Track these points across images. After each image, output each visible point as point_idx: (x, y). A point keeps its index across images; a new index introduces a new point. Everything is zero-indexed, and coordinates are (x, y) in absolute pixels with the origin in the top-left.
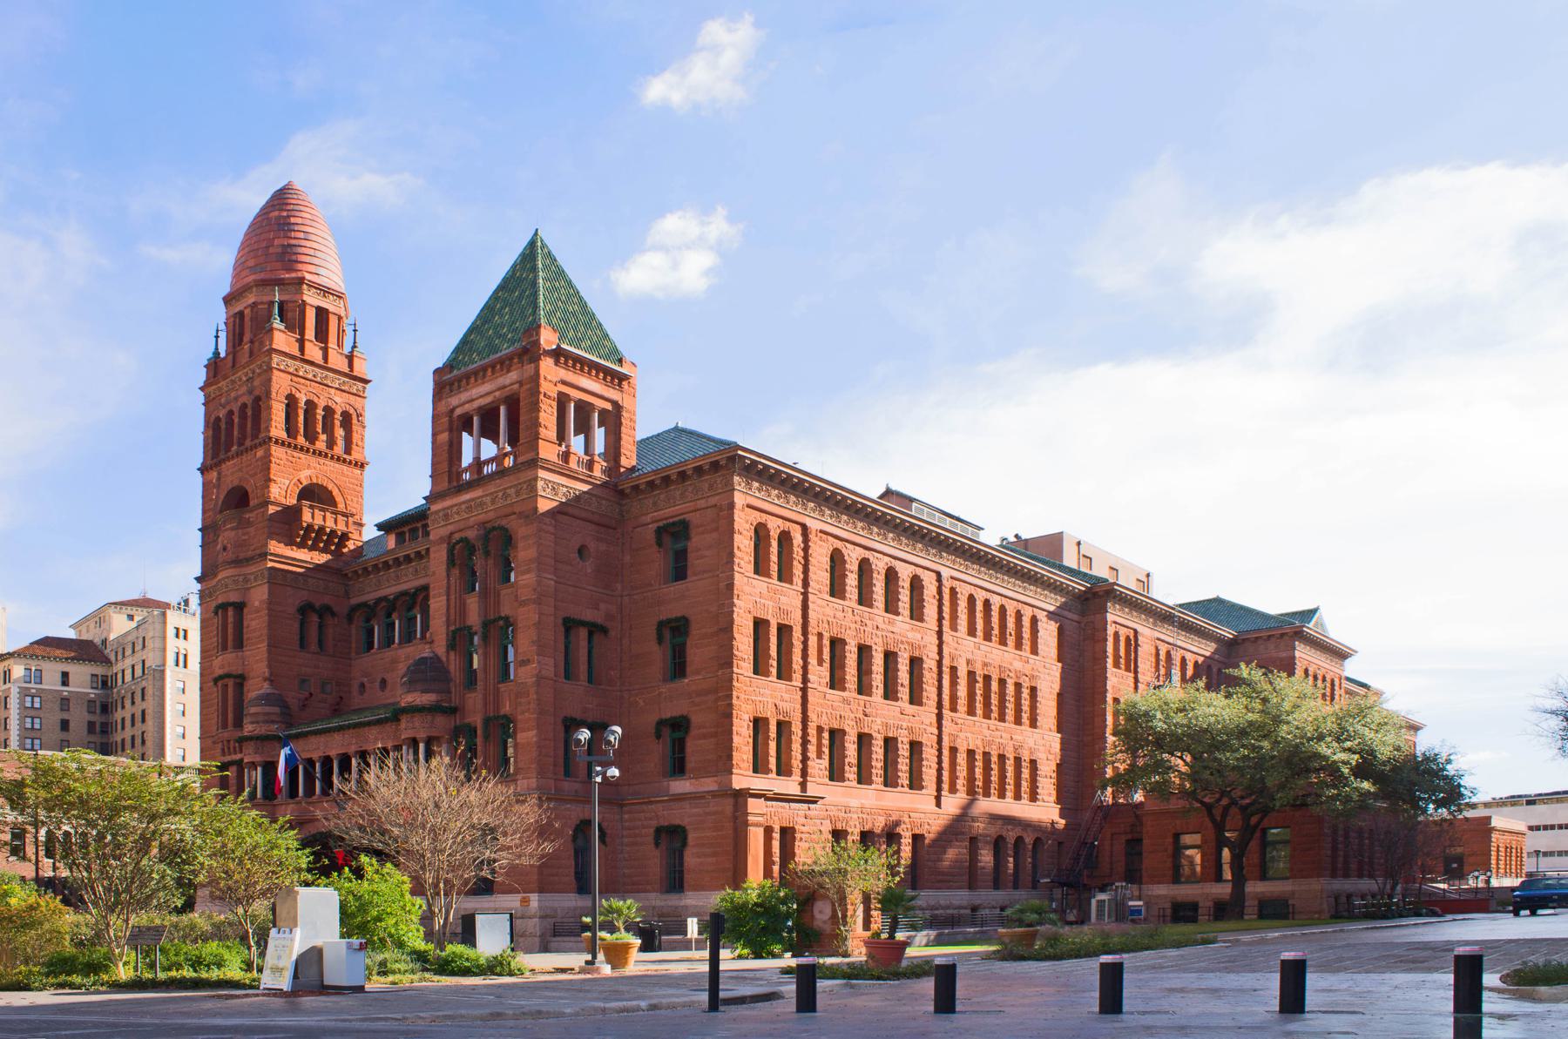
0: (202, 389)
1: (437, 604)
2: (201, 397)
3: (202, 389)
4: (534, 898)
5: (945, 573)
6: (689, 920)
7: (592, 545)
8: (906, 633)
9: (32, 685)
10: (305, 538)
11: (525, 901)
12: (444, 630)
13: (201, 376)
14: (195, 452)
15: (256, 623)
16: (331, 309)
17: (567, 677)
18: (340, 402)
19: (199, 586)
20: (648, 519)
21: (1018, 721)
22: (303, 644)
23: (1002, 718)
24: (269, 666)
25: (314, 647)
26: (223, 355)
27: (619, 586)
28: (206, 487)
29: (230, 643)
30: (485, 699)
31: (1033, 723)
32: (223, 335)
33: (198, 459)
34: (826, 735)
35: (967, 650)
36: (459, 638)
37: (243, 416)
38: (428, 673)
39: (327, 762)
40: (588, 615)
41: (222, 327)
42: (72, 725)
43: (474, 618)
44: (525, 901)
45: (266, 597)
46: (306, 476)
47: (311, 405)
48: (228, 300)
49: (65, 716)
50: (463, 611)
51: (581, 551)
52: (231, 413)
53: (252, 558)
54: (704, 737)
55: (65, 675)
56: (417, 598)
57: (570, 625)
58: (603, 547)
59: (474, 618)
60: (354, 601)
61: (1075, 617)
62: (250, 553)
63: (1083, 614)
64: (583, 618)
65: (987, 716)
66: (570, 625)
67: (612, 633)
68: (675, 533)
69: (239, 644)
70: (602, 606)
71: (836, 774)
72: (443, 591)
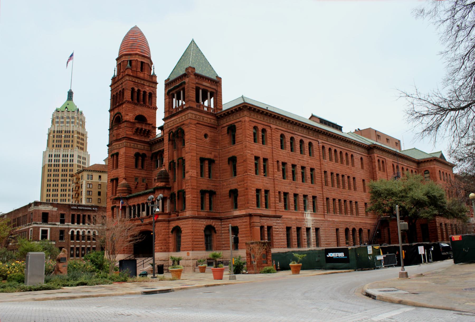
0: (110, 86)
1: (166, 154)
2: (110, 89)
3: (110, 86)
4: (191, 252)
5: (320, 141)
6: (371, 253)
7: (209, 134)
8: (305, 160)
9: (90, 180)
10: (144, 133)
11: (188, 254)
12: (167, 162)
13: (110, 82)
14: (108, 105)
15: (121, 159)
16: (145, 62)
17: (201, 176)
18: (147, 89)
19: (108, 148)
20: (225, 125)
21: (350, 188)
22: (136, 166)
23: (344, 187)
24: (125, 174)
25: (140, 167)
26: (116, 75)
27: (218, 146)
28: (110, 115)
29: (115, 167)
30: (178, 184)
31: (355, 189)
32: (116, 70)
33: (109, 108)
34: (282, 195)
35: (330, 166)
36: (172, 165)
37: (120, 95)
38: (164, 177)
39: (139, 205)
40: (208, 156)
41: (116, 68)
42: (101, 193)
43: (176, 159)
44: (188, 254)
45: (124, 151)
46: (138, 113)
47: (139, 91)
48: (117, 59)
49: (100, 190)
50: (173, 156)
51: (206, 136)
52: (117, 93)
53: (121, 139)
54: (242, 196)
55: (100, 177)
56: (162, 152)
57: (202, 160)
58: (213, 134)
59: (176, 159)
60: (153, 152)
61: (366, 155)
62: (120, 137)
63: (368, 154)
64: (206, 157)
65: (339, 187)
66: (202, 160)
67: (216, 162)
68: (232, 129)
69: (117, 167)
70: (213, 153)
71: (286, 207)
72: (167, 149)
